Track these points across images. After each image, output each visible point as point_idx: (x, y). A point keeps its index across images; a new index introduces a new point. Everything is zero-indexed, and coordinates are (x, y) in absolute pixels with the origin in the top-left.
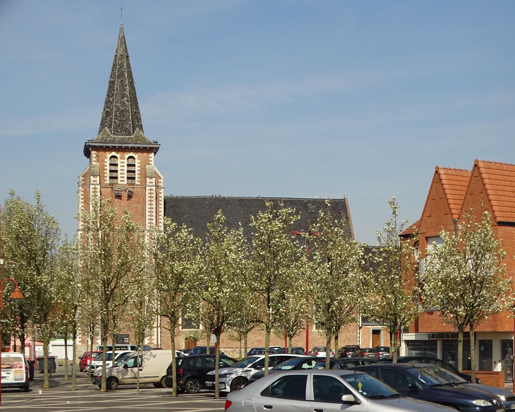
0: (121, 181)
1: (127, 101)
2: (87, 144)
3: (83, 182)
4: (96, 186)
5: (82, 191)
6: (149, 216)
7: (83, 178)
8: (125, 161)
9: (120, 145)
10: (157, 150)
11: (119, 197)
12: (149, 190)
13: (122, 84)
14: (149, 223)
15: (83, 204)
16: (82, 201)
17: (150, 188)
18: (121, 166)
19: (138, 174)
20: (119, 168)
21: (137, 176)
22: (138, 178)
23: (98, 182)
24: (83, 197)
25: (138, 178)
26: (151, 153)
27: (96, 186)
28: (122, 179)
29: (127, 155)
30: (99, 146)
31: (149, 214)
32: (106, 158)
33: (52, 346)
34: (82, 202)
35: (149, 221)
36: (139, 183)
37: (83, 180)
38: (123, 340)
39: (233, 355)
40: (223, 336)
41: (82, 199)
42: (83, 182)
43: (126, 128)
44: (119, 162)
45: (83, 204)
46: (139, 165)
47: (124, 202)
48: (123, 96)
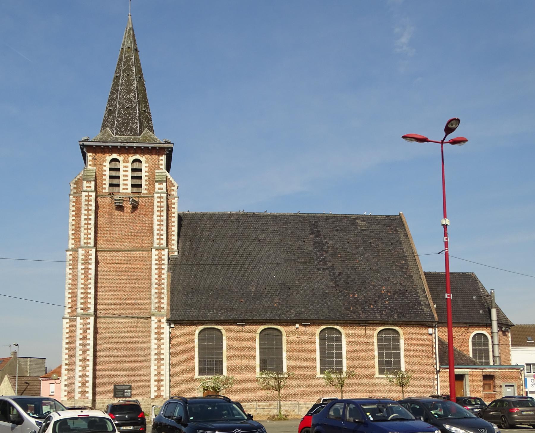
0: (123, 189)
1: (135, 97)
3: (75, 191)
4: (90, 194)
5: (74, 202)
7: (75, 186)
9: (122, 145)
11: (120, 208)
15: (74, 218)
21: (144, 183)
26: (162, 155)
27: (90, 194)
31: (158, 227)
32: (105, 161)
34: (73, 215)
35: (158, 237)
37: (75, 188)
38: (124, 392)
41: (73, 211)
42: (75, 191)
44: (121, 166)
45: (74, 218)
47: (127, 215)
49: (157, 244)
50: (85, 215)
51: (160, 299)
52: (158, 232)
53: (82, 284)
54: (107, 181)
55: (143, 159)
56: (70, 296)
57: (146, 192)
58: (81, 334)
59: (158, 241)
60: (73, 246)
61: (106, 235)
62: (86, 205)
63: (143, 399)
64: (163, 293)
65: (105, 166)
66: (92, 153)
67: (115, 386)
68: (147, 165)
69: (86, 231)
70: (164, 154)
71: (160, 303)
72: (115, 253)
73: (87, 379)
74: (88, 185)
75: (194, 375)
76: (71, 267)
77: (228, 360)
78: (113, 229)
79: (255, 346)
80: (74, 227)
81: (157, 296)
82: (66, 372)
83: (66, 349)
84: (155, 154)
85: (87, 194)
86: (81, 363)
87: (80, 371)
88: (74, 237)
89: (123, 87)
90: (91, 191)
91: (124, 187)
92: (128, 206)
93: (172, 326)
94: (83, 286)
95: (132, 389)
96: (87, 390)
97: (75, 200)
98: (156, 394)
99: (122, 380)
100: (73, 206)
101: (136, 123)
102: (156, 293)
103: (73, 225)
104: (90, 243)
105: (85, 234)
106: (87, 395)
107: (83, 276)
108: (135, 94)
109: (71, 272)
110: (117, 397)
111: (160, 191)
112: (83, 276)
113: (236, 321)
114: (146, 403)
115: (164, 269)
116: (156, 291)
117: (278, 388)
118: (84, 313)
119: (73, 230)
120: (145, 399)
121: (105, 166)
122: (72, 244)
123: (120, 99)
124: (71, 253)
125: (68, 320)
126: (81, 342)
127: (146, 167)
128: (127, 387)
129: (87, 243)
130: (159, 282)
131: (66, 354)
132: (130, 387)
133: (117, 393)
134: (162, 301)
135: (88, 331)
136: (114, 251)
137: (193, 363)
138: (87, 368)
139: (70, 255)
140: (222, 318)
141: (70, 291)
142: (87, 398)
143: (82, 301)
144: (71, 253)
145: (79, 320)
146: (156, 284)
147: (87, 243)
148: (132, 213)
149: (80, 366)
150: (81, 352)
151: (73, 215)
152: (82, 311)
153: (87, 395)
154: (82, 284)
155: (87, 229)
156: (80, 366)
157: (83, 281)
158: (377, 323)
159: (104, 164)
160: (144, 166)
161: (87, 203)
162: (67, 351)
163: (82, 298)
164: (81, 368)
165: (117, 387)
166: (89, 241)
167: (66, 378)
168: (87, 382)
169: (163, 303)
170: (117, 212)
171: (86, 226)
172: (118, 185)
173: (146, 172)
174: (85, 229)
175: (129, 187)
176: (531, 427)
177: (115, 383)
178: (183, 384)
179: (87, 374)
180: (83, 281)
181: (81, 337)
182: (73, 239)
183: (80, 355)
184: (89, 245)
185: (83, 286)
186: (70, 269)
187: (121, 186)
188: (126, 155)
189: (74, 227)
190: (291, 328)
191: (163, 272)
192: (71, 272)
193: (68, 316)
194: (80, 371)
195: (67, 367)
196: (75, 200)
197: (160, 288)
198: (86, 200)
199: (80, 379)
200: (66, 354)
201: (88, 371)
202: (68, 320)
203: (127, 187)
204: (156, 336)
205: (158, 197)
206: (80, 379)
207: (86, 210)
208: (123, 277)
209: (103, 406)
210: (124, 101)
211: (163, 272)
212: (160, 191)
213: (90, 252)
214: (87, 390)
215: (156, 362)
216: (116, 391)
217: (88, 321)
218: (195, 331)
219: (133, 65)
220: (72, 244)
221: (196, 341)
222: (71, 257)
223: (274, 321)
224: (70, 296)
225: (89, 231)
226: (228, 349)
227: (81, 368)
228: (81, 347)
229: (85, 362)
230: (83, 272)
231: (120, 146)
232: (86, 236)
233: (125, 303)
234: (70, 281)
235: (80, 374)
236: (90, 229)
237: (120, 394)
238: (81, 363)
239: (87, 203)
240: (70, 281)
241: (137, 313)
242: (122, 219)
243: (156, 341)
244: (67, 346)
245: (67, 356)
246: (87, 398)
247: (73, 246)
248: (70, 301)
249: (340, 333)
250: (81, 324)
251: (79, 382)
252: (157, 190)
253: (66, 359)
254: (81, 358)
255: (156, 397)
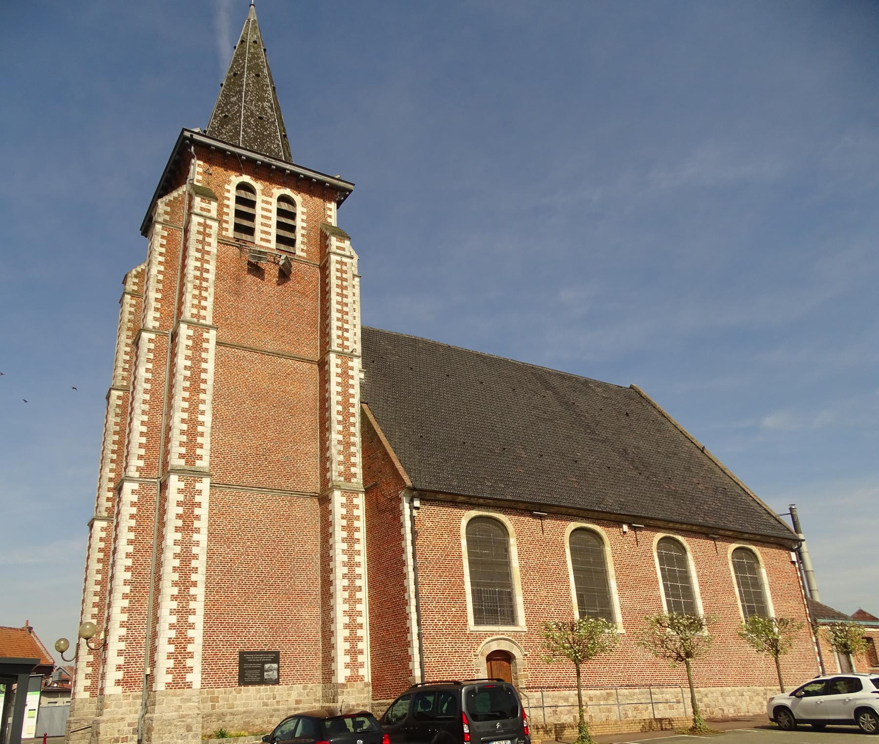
0: (262, 239)
1: (271, 108)
3: (167, 217)
4: (209, 222)
5: (163, 237)
7: (168, 209)
9: (266, 160)
10: (346, 197)
11: (255, 269)
14: (339, 337)
15: (162, 268)
17: (339, 258)
19: (303, 235)
20: (258, 211)
21: (299, 239)
22: (302, 243)
23: (214, 214)
24: (163, 250)
26: (330, 201)
27: (209, 222)
28: (264, 236)
29: (278, 191)
30: (217, 148)
32: (229, 182)
34: (160, 263)
37: (166, 213)
38: (262, 671)
39: (258, 692)
41: (161, 254)
42: (167, 217)
43: (269, 148)
44: (259, 198)
45: (162, 268)
47: (270, 284)
48: (262, 99)
49: (339, 345)
51: (348, 456)
53: (184, 399)
55: (298, 198)
57: (304, 254)
58: (179, 516)
60: (157, 324)
61: (228, 316)
62: (198, 241)
63: (305, 688)
64: (354, 444)
66: (204, 162)
67: (242, 654)
68: (305, 210)
69: (197, 292)
70: (335, 201)
72: (246, 354)
73: (190, 633)
74: (204, 205)
75: (465, 625)
76: (150, 366)
77: (525, 591)
79: (565, 562)
80: (160, 286)
81: (341, 447)
82: (125, 617)
85: (202, 220)
87: (172, 612)
88: (159, 306)
92: (272, 272)
93: (417, 503)
94: (186, 405)
95: (282, 660)
96: (189, 662)
98: (348, 672)
100: (162, 246)
102: (339, 442)
103: (159, 281)
104: (204, 318)
105: (194, 297)
106: (189, 677)
107: (187, 384)
110: (247, 684)
111: (338, 251)
112: (187, 384)
113: (530, 507)
114: (312, 697)
115: (353, 396)
116: (341, 437)
117: (685, 656)
118: (187, 467)
119: (158, 291)
120: (310, 685)
122: (155, 319)
124: (153, 336)
125: (136, 486)
128: (271, 656)
129: (198, 316)
130: (344, 419)
131: (127, 569)
132: (275, 658)
134: (353, 459)
136: (245, 348)
137: (463, 593)
139: (150, 341)
140: (509, 498)
142: (190, 687)
143: (184, 438)
144: (153, 336)
147: (198, 316)
148: (279, 285)
149: (174, 598)
151: (160, 263)
152: (182, 462)
153: (189, 677)
154: (184, 399)
155: (200, 288)
156: (174, 598)
157: (187, 395)
158: (729, 537)
161: (201, 237)
162: (129, 562)
164: (174, 605)
165: (248, 657)
166: (203, 313)
167: (123, 631)
168: (191, 641)
169: (354, 465)
170: (250, 278)
171: (198, 282)
174: (195, 287)
175: (273, 238)
177: (242, 648)
180: (187, 395)
181: (180, 523)
182: (156, 309)
183: (175, 569)
184: (202, 321)
185: (186, 405)
186: (147, 370)
188: (267, 183)
189: (160, 286)
190: (615, 531)
192: (149, 376)
193: (137, 475)
194: (172, 612)
195: (126, 603)
196: (165, 234)
198: (199, 232)
199: (173, 634)
200: (127, 569)
201: (194, 613)
202: (136, 486)
203: (268, 237)
204: (345, 534)
205: (337, 262)
208: (263, 405)
209: (213, 707)
210: (253, 108)
211: (351, 400)
213: (205, 335)
214: (189, 662)
216: (246, 666)
217: (198, 486)
218: (460, 519)
220: (155, 319)
221: (464, 542)
222: (152, 346)
223: (590, 515)
226: (522, 567)
227: (174, 605)
229: (187, 588)
230: (188, 373)
231: (263, 162)
232: (196, 302)
233: (266, 459)
235: (174, 619)
236: (206, 289)
238: (175, 591)
240: (147, 397)
241: (291, 484)
243: (345, 546)
245: (128, 576)
246: (190, 687)
247: (157, 324)
249: (683, 549)
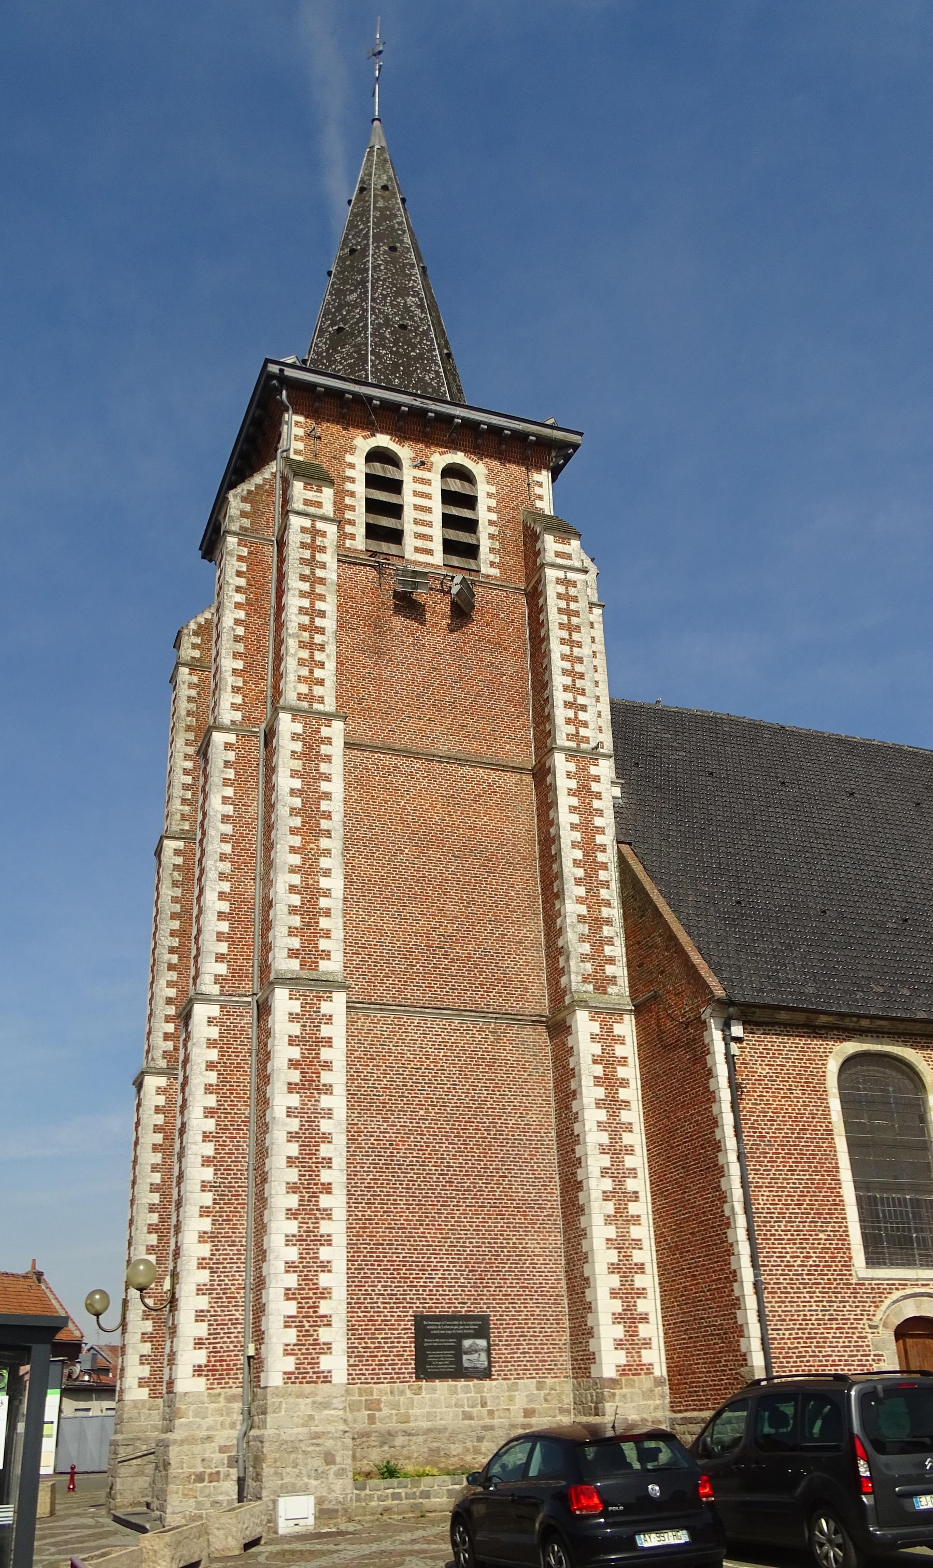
0: (417, 550)
1: (421, 306)
2: (274, 369)
3: (246, 522)
4: (320, 525)
5: (240, 558)
6: (566, 689)
7: (248, 507)
8: (435, 477)
9: (418, 403)
10: (567, 458)
11: (408, 605)
12: (559, 581)
13: (394, 261)
15: (241, 615)
16: (240, 598)
18: (416, 494)
19: (491, 537)
20: (408, 499)
21: (485, 544)
25: (491, 550)
26: (539, 469)
27: (320, 525)
31: (568, 681)
32: (352, 450)
33: (52, 1423)
34: (238, 605)
35: (570, 713)
36: (495, 572)
38: (459, 1352)
40: (243, 1359)
41: (238, 589)
42: (246, 522)
43: (421, 380)
45: (241, 615)
46: (493, 503)
47: (435, 633)
48: (403, 292)
49: (569, 737)
50: (302, 594)
51: (599, 943)
52: (569, 697)
54: (359, 516)
56: (225, 906)
57: (495, 572)
58: (293, 1064)
59: (571, 729)
65: (352, 466)
66: (306, 417)
67: (419, 1320)
68: (493, 490)
69: (305, 654)
70: (547, 468)
71: (598, 958)
72: (400, 761)
73: (324, 1280)
78: (386, 674)
80: (240, 647)
81: (584, 928)
82: (205, 1250)
83: (206, 1137)
84: (518, 463)
86: (293, 1201)
89: (382, 275)
90: (325, 519)
91: (420, 543)
92: (439, 609)
93: (737, 1030)
94: (296, 860)
95: (494, 1333)
96: (324, 1334)
97: (245, 552)
98: (621, 1357)
99: (450, 1296)
100: (239, 574)
101: (437, 372)
103: (237, 639)
104: (321, 700)
106: (325, 1363)
108: (421, 299)
109: (229, 809)
118: (304, 974)
119: (236, 655)
121: (352, 466)
123: (373, 300)
124: (232, 738)
125: (214, 1010)
126: (294, 1100)
127: (489, 495)
128: (473, 1325)
129: (309, 697)
133: (432, 1356)
135: (325, 1054)
137: (839, 1204)
138: (325, 1227)
141: (226, 887)
145: (283, 1002)
146: (578, 882)
149: (291, 1214)
150: (293, 1149)
151: (238, 605)
152: (295, 964)
153: (325, 1363)
154: (293, 850)
155: (310, 646)
156: (291, 1214)
159: (349, 458)
160: (483, 490)
161: (307, 554)
162: (209, 1149)
163: (293, 910)
164: (292, 1227)
165: (431, 1326)
170: (399, 622)
171: (306, 635)
172: (396, 536)
173: (490, 509)
175: (437, 546)
176: (927, 1476)
178: (812, 1305)
179: (324, 1253)
183: (291, 1161)
187: (409, 542)
191: (600, 839)
192: (229, 809)
193: (215, 990)
195: (206, 1224)
196: (245, 552)
197: (593, 901)
199: (292, 1280)
201: (329, 1243)
202: (214, 1010)
205: (559, 581)
206: (292, 1280)
207: (303, 578)
210: (387, 309)
211: (600, 839)
212: (559, 561)
215: (610, 1208)
216: (428, 1342)
217: (325, 1007)
218: (824, 1059)
219: (404, 232)
221: (835, 1105)
222: (231, 756)
224: (225, 906)
225: (319, 656)
227: (292, 1227)
228: (294, 1124)
229: (314, 1195)
231: (411, 407)
233: (446, 955)
234: (227, 848)
235: (292, 1253)
236: (322, 648)
237: (442, 1360)
238: (293, 1201)
239: (307, 554)
242: (418, 645)
244: (210, 1125)
245: (208, 1174)
247: (238, 716)
248: (224, 927)
250: (293, 1018)
251: (289, 1295)
252: (550, 557)
253: (205, 1186)
254: (293, 1175)
255: (624, 1371)
